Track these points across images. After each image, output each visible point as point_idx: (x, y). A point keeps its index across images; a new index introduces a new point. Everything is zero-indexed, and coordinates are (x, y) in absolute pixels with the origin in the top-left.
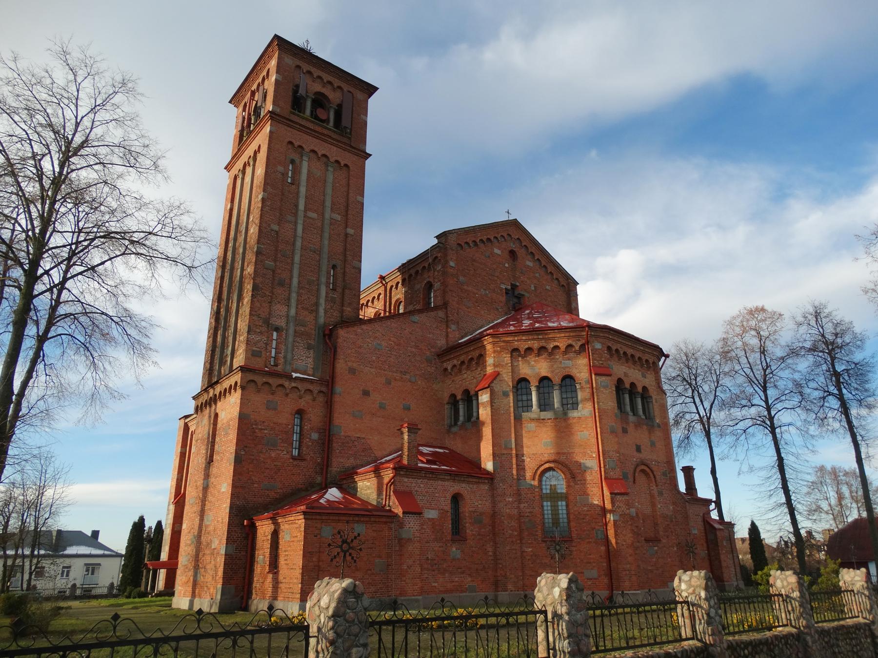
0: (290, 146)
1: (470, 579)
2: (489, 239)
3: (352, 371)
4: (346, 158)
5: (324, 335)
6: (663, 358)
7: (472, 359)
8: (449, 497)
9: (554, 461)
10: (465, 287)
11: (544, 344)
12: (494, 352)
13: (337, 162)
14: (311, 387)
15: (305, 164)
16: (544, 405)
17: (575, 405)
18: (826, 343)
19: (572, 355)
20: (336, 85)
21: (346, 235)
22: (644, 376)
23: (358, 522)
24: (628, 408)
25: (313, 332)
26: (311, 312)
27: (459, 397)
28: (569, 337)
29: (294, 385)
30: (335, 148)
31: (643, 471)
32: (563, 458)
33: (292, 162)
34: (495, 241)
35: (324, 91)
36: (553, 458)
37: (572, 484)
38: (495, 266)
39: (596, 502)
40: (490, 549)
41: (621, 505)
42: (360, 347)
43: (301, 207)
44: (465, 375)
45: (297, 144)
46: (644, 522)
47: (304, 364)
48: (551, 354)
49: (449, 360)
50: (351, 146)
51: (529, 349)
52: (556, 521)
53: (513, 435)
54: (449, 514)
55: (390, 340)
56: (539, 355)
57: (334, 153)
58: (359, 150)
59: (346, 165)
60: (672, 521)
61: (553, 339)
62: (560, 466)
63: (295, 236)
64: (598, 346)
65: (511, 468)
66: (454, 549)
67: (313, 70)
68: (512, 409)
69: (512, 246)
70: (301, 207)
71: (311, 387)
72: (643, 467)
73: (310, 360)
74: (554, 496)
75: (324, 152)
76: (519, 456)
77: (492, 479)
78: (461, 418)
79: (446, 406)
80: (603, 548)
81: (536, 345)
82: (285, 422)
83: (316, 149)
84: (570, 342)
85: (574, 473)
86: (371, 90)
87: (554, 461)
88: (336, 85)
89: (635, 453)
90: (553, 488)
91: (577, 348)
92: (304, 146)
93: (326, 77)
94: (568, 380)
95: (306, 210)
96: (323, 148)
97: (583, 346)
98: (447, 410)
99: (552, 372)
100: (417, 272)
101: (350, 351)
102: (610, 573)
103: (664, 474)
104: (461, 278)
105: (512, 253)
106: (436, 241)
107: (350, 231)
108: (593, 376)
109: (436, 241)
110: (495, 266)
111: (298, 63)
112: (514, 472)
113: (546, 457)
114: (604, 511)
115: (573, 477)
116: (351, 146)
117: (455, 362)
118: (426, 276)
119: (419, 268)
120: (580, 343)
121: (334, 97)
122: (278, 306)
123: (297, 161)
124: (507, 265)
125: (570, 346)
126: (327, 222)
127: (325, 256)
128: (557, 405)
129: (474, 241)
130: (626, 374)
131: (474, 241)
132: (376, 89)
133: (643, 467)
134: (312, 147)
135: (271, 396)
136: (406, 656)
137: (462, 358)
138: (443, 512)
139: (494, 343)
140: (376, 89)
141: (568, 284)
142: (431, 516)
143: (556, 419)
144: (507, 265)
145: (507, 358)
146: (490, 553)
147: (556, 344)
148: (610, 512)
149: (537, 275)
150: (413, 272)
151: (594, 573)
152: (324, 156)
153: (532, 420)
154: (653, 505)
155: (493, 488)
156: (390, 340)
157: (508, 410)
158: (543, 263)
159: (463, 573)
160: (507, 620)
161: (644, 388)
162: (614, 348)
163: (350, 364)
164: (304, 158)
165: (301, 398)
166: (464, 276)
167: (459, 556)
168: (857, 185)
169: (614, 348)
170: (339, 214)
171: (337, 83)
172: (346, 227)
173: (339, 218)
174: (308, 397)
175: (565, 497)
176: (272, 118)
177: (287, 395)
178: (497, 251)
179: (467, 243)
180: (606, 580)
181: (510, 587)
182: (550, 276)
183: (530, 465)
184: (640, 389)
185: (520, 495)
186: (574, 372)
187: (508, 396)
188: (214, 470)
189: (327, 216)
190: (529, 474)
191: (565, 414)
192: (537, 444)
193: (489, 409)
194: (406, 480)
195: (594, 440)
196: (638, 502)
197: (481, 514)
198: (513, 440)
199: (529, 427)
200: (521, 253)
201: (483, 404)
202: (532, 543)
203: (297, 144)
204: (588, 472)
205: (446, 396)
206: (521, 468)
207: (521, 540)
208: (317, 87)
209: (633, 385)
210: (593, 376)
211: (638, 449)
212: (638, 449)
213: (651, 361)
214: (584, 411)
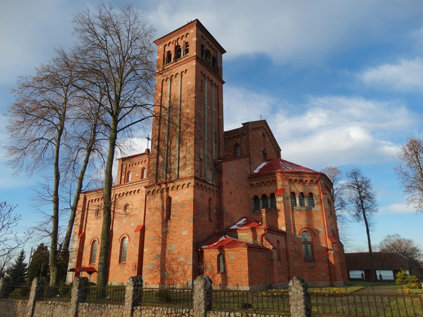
5: (215, 165)
9: (307, 228)
11: (302, 179)
12: (282, 180)
16: (302, 204)
17: (313, 206)
18: (358, 185)
19: (312, 184)
23: (259, 251)
28: (311, 177)
32: (310, 227)
33: (202, 80)
36: (306, 227)
37: (315, 238)
39: (324, 246)
44: (264, 188)
47: (209, 176)
48: (304, 183)
49: (254, 180)
51: (296, 180)
52: (307, 253)
53: (291, 216)
56: (299, 183)
61: (305, 177)
62: (309, 230)
64: (322, 182)
65: (291, 230)
68: (290, 205)
73: (211, 175)
74: (306, 242)
76: (294, 225)
77: (286, 234)
80: (327, 264)
81: (298, 179)
84: (312, 179)
85: (314, 233)
87: (307, 228)
90: (305, 239)
91: (315, 182)
94: (311, 194)
97: (317, 181)
98: (252, 202)
99: (305, 191)
100: (230, 138)
102: (330, 275)
105: (264, 134)
106: (242, 126)
108: (322, 194)
109: (242, 126)
112: (293, 232)
113: (304, 226)
114: (327, 249)
115: (315, 235)
117: (258, 182)
118: (235, 140)
119: (232, 136)
120: (316, 180)
125: (312, 181)
128: (306, 205)
132: (225, 52)
135: (202, 191)
136: (132, 315)
137: (262, 180)
139: (281, 176)
140: (225, 52)
141: (278, 150)
143: (307, 210)
145: (287, 183)
147: (306, 179)
148: (331, 250)
150: (227, 137)
151: (324, 274)
153: (298, 210)
155: (286, 239)
157: (289, 205)
160: (229, 294)
164: (206, 80)
168: (302, 111)
172: (218, 115)
175: (311, 243)
176: (196, 59)
180: (329, 278)
183: (298, 229)
185: (294, 241)
186: (313, 192)
187: (288, 199)
188: (172, 224)
190: (297, 233)
191: (311, 209)
192: (300, 221)
193: (282, 204)
195: (322, 221)
198: (291, 218)
199: (297, 213)
201: (278, 202)
204: (320, 233)
205: (252, 196)
206: (295, 230)
210: (322, 194)
214: (317, 208)
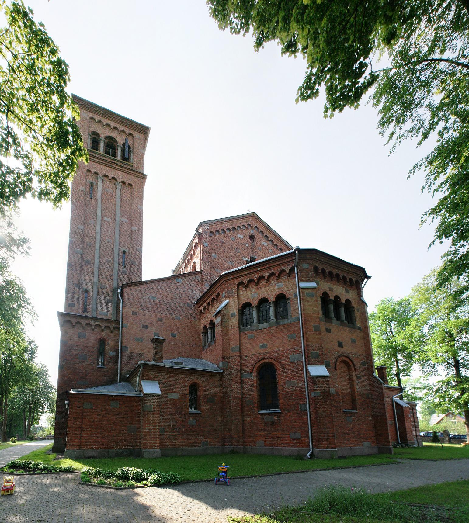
0: (89, 174)
1: (203, 438)
2: (234, 228)
3: (135, 313)
4: (129, 179)
6: (366, 279)
7: (213, 299)
8: (188, 385)
10: (216, 260)
13: (123, 182)
14: (109, 325)
15: (100, 185)
20: (120, 130)
21: (132, 231)
22: (347, 291)
24: (332, 315)
25: (111, 293)
26: (109, 280)
27: (208, 327)
29: (97, 323)
30: (121, 173)
31: (344, 362)
34: (239, 229)
35: (112, 135)
38: (239, 246)
40: (220, 419)
41: (322, 385)
42: (140, 299)
43: (99, 214)
45: (93, 171)
46: (343, 398)
50: (132, 170)
54: (188, 396)
55: (161, 294)
57: (121, 176)
58: (137, 172)
59: (130, 185)
60: (368, 398)
63: (96, 233)
66: (191, 419)
67: (102, 119)
69: (252, 232)
70: (99, 214)
71: (109, 325)
72: (344, 358)
75: (113, 176)
78: (209, 340)
79: (202, 335)
82: (91, 345)
83: (107, 174)
86: (144, 131)
88: (120, 130)
89: (337, 348)
92: (98, 172)
93: (113, 124)
95: (102, 216)
96: (112, 173)
101: (133, 301)
103: (363, 364)
104: (213, 255)
105: (252, 237)
107: (134, 228)
110: (239, 246)
111: (91, 115)
116: (134, 171)
121: (120, 139)
122: (86, 277)
123: (95, 183)
124: (247, 245)
126: (118, 223)
127: (117, 245)
129: (223, 230)
130: (331, 289)
131: (223, 230)
133: (344, 358)
134: (104, 173)
138: (183, 396)
142: (172, 397)
144: (247, 245)
146: (220, 421)
149: (270, 251)
152: (114, 178)
154: (352, 386)
156: (161, 294)
158: (275, 243)
159: (198, 434)
161: (348, 301)
162: (320, 267)
163: (133, 309)
165: (102, 331)
166: (216, 253)
167: (194, 424)
169: (320, 267)
170: (126, 218)
171: (121, 127)
172: (132, 225)
173: (127, 221)
174: (108, 331)
177: (93, 329)
178: (240, 236)
179: (217, 231)
181: (234, 443)
182: (275, 247)
184: (343, 301)
189: (118, 219)
194: (153, 373)
196: (338, 384)
197: (213, 396)
200: (258, 236)
202: (250, 415)
203: (93, 171)
207: (243, 412)
208: (108, 133)
209: (337, 298)
211: (340, 345)
212: (340, 345)
213: (354, 280)
